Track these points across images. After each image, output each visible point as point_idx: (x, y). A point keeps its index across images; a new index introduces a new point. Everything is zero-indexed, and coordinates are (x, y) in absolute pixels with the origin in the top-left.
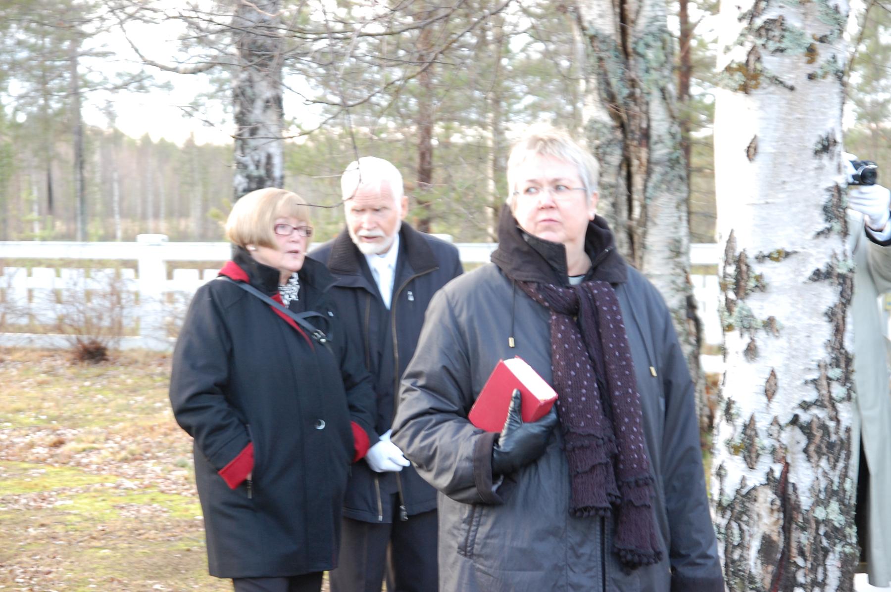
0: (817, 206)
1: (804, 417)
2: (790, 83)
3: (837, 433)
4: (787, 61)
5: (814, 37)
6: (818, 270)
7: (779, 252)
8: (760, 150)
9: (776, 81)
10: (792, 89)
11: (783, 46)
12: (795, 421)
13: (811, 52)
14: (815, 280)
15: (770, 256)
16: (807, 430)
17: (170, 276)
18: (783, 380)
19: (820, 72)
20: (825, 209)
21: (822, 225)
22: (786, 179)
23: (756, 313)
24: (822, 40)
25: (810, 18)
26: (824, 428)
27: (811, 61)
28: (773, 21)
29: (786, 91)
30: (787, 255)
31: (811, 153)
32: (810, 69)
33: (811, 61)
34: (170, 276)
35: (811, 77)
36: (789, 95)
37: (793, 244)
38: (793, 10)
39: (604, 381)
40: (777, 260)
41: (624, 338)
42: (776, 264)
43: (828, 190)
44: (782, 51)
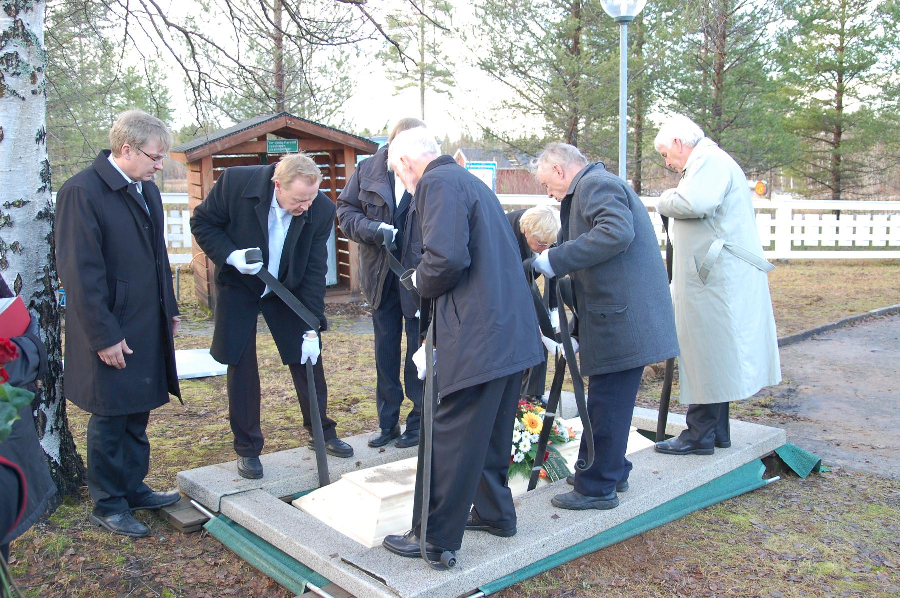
0: (38, 173)
1: (38, 301)
2: (22, 95)
3: (55, 309)
4: (21, 81)
5: (34, 67)
6: (41, 212)
7: (20, 202)
8: (5, 137)
9: (14, 93)
10: (24, 99)
11: (18, 71)
12: (32, 304)
13: (34, 77)
14: (40, 219)
15: (14, 204)
16: (39, 309)
17: (773, 242)
18: (25, 281)
19: (39, 90)
20: (42, 174)
21: (41, 185)
22: (22, 156)
23: (6, 240)
24: (39, 70)
25: (32, 56)
26: (49, 307)
27: (34, 83)
28: (12, 55)
29: (21, 100)
30: (25, 203)
31: (34, 140)
32: (33, 88)
33: (34, 83)
34: (773, 242)
35: (34, 93)
36: (22, 103)
37: (27, 196)
38: (23, 49)
39: (56, 336)
40: (19, 206)
41: (322, 303)
42: (18, 209)
43: (42, 163)
44: (19, 75)
